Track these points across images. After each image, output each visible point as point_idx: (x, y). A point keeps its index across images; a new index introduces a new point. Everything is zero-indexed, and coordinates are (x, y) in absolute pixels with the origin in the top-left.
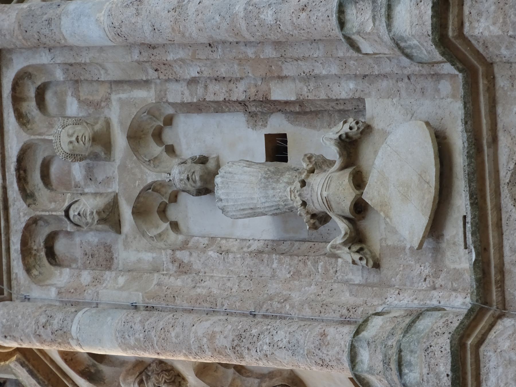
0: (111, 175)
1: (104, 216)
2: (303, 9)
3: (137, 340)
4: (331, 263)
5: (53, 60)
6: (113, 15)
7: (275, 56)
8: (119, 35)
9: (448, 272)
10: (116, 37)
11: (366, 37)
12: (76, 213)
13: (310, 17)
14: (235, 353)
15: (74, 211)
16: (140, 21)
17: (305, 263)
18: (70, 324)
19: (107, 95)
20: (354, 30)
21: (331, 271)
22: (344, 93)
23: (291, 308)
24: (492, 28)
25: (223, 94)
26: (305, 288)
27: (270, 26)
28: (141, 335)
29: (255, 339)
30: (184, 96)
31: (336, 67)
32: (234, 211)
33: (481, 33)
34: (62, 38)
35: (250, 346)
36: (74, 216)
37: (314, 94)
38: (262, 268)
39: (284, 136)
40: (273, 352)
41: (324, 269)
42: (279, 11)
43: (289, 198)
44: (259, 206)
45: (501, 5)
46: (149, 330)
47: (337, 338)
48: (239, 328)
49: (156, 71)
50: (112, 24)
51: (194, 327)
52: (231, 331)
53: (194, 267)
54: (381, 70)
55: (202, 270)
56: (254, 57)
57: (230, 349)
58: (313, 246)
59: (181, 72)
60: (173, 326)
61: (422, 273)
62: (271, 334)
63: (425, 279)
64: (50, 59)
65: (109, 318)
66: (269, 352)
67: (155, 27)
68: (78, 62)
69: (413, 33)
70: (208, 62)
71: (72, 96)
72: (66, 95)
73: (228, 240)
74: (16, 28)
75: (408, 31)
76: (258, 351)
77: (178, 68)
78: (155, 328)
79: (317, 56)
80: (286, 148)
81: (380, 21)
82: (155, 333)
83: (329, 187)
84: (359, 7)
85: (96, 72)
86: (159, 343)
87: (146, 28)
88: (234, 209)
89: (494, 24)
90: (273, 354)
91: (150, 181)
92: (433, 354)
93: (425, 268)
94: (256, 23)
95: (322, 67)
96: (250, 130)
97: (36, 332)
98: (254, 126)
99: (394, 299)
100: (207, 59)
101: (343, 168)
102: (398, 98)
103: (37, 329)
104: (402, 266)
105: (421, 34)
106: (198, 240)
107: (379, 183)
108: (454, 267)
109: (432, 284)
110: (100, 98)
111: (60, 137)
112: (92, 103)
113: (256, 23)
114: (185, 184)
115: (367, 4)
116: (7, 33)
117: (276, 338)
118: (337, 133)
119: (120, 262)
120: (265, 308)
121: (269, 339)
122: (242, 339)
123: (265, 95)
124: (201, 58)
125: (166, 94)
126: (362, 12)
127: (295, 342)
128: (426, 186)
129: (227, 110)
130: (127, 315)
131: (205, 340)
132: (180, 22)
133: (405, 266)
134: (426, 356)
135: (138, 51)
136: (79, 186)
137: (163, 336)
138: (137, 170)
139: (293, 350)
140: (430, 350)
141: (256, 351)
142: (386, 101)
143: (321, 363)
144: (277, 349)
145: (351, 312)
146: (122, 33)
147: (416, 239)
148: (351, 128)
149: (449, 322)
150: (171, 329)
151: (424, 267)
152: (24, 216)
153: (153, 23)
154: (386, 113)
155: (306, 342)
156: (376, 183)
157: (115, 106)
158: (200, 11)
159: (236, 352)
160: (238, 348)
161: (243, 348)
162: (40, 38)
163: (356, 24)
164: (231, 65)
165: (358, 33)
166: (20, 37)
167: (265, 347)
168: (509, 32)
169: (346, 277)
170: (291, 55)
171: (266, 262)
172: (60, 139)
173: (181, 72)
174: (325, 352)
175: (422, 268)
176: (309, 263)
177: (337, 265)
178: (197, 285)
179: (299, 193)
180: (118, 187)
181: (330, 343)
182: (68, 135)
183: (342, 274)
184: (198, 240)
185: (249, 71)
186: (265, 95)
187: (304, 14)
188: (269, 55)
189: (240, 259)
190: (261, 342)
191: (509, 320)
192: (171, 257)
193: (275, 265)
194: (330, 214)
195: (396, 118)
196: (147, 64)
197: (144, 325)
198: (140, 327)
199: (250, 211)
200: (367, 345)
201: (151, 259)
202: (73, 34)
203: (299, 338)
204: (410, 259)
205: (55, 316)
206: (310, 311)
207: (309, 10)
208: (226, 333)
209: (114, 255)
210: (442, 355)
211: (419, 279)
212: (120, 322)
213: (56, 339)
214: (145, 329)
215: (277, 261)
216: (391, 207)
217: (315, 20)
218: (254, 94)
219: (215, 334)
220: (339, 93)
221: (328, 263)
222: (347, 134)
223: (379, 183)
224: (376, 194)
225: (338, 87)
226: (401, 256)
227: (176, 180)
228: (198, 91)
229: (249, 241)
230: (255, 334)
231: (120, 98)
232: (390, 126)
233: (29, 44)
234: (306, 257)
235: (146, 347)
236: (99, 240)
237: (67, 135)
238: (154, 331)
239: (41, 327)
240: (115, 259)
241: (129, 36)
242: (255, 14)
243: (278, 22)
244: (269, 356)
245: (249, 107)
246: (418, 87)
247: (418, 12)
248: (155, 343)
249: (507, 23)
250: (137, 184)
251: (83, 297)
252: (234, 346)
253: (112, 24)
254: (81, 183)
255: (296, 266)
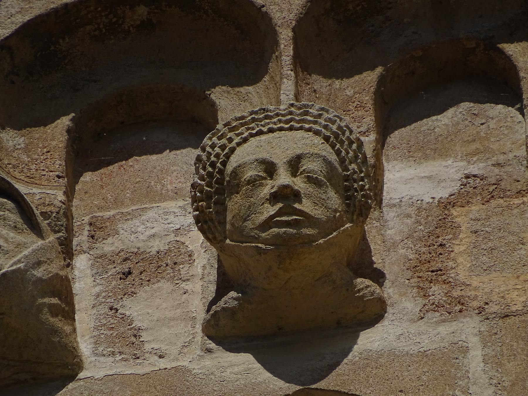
0: (148, 347)
19: (475, 304)
71: (467, 177)
72: (468, 157)
111: (291, 129)
136: (98, 234)
172: (281, 129)
180: (100, 374)
231: (465, 350)
237: (299, 152)
254: (110, 240)
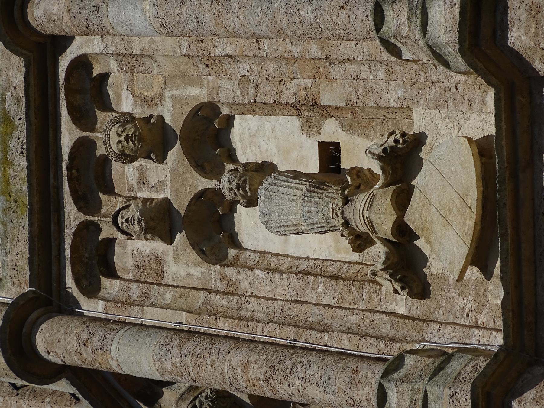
0: (163, 179)
1: (152, 224)
2: (343, 7)
3: (173, 364)
4: (376, 291)
5: (105, 50)
6: (158, 4)
7: (320, 56)
8: (164, 26)
9: (490, 308)
10: (161, 29)
11: (404, 41)
12: (124, 220)
13: (349, 16)
14: (268, 385)
15: (122, 218)
16: (184, 13)
17: (350, 291)
18: (110, 343)
19: (161, 91)
20: (391, 33)
21: (375, 300)
22: (392, 100)
23: (330, 339)
24: (524, 38)
25: (273, 96)
26: (347, 317)
27: (310, 24)
28: (178, 360)
29: (288, 371)
30: (235, 96)
31: (383, 71)
32: (278, 227)
33: (513, 43)
34: (109, 26)
35: (283, 381)
36: (122, 223)
37: (363, 101)
38: (307, 292)
39: (338, 144)
40: (305, 387)
41: (368, 296)
42: (319, 8)
43: (331, 216)
44: (302, 223)
45: (533, 12)
46: (185, 354)
47: (368, 376)
48: (273, 358)
49: (206, 67)
50: (158, 13)
51: (230, 354)
52: (265, 362)
53: (241, 285)
54: (428, 78)
55: (249, 290)
56: (299, 57)
57: (263, 381)
58: (361, 269)
59: (231, 69)
60: (209, 353)
61: (465, 307)
62: (304, 367)
63: (468, 315)
64: (102, 48)
65: (149, 339)
66: (301, 387)
67: (199, 20)
68: (129, 53)
69: (447, 39)
70: (257, 60)
71: (127, 89)
73: (279, 257)
74: (66, 13)
75: (441, 36)
76: (291, 385)
77: (228, 65)
78: (192, 353)
79: (361, 59)
80: (339, 158)
81: (416, 24)
82: (191, 358)
83: (371, 205)
84: (396, 7)
85: (149, 64)
86: (195, 370)
87: (189, 20)
88: (277, 225)
89: (526, 34)
90: (305, 389)
91: (200, 188)
92: (457, 402)
93: (468, 302)
94: (297, 20)
95: (369, 71)
96: (304, 136)
97: (77, 350)
98: (308, 134)
99: (434, 336)
100: (255, 57)
101: (386, 185)
102: (446, 110)
103: (78, 347)
104: (445, 298)
105: (454, 41)
106: (249, 256)
107: (421, 204)
108: (496, 303)
109: (474, 320)
110: (154, 94)
111: (109, 135)
112: (146, 99)
113: (297, 20)
114: (235, 194)
115: (403, 5)
116: (56, 18)
117: (309, 372)
118: (381, 146)
119: (170, 276)
120: (304, 337)
121: (302, 373)
122: (275, 371)
123: (314, 99)
124: (248, 55)
125: (218, 93)
126: (399, 13)
127: (327, 378)
128: (468, 210)
129: (280, 113)
130: (166, 337)
131: (239, 369)
132: (222, 15)
133: (448, 298)
134: (451, 404)
135: (187, 44)
136: (132, 190)
137: (198, 363)
138: (188, 176)
139: (325, 386)
140: (455, 396)
141: (289, 386)
142: (433, 112)
143: (352, 402)
144: (309, 385)
145: (389, 347)
146: (167, 25)
147: (457, 269)
148: (396, 141)
149: (478, 366)
150: (207, 355)
151: (467, 300)
152: (74, 221)
153: (197, 15)
154: (433, 126)
155: (337, 379)
156: (418, 204)
157: (168, 102)
158: (243, 4)
159: (269, 385)
160: (271, 381)
161: (276, 381)
162: (89, 26)
163: (393, 26)
164: (280, 64)
165: (395, 36)
166: (69, 24)
167: (298, 382)
168: (541, 44)
169: (390, 307)
170: (336, 56)
171: (312, 285)
172: (109, 138)
173: (231, 69)
174: (356, 392)
175: (465, 301)
176: (354, 289)
177: (381, 293)
178: (242, 306)
179: (341, 210)
181: (361, 382)
182: (117, 134)
183: (386, 304)
184: (249, 256)
185: (298, 72)
186: (314, 99)
187: (344, 12)
188: (314, 56)
189: (286, 280)
190: (293, 376)
191: (539, 368)
192: (220, 274)
193: (320, 290)
194: (373, 236)
195: (443, 132)
196: (197, 59)
197: (181, 350)
198: (178, 351)
199: (293, 228)
200: (395, 386)
201: (200, 275)
202: (120, 23)
203: (331, 373)
204: (454, 290)
205: (96, 333)
206: (348, 343)
207: (349, 8)
208: (260, 363)
209: (165, 268)
210: (466, 404)
211: (462, 313)
212: (158, 344)
213: (96, 359)
214: (182, 353)
215: (322, 284)
216: (432, 233)
217: (354, 19)
218: (304, 98)
219: (250, 364)
220: (388, 101)
221: (372, 290)
222: (391, 147)
223: (421, 204)
224: (418, 216)
225: (387, 95)
226: (445, 287)
227: (225, 188)
228: (249, 90)
229: (300, 259)
230: (289, 367)
231: (173, 95)
232: (437, 141)
233: (79, 31)
234: (351, 282)
235: (182, 373)
236: (150, 250)
237: (116, 134)
238: (191, 356)
239: (82, 345)
240: (165, 272)
241: (174, 28)
242: (296, 9)
243: (318, 20)
244: (301, 391)
245: (302, 111)
246: (465, 98)
247: (452, 16)
248: (191, 369)
249: (539, 34)
250: (188, 191)
251: (129, 313)
252: (267, 378)
253: (158, 13)
255: (341, 291)
